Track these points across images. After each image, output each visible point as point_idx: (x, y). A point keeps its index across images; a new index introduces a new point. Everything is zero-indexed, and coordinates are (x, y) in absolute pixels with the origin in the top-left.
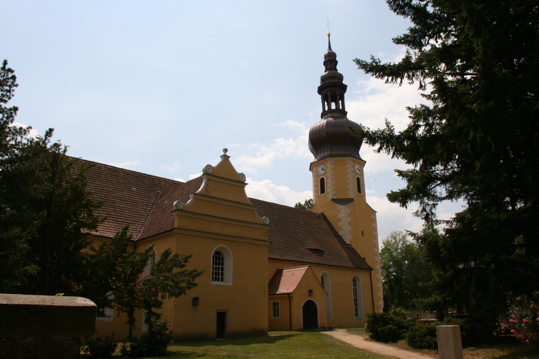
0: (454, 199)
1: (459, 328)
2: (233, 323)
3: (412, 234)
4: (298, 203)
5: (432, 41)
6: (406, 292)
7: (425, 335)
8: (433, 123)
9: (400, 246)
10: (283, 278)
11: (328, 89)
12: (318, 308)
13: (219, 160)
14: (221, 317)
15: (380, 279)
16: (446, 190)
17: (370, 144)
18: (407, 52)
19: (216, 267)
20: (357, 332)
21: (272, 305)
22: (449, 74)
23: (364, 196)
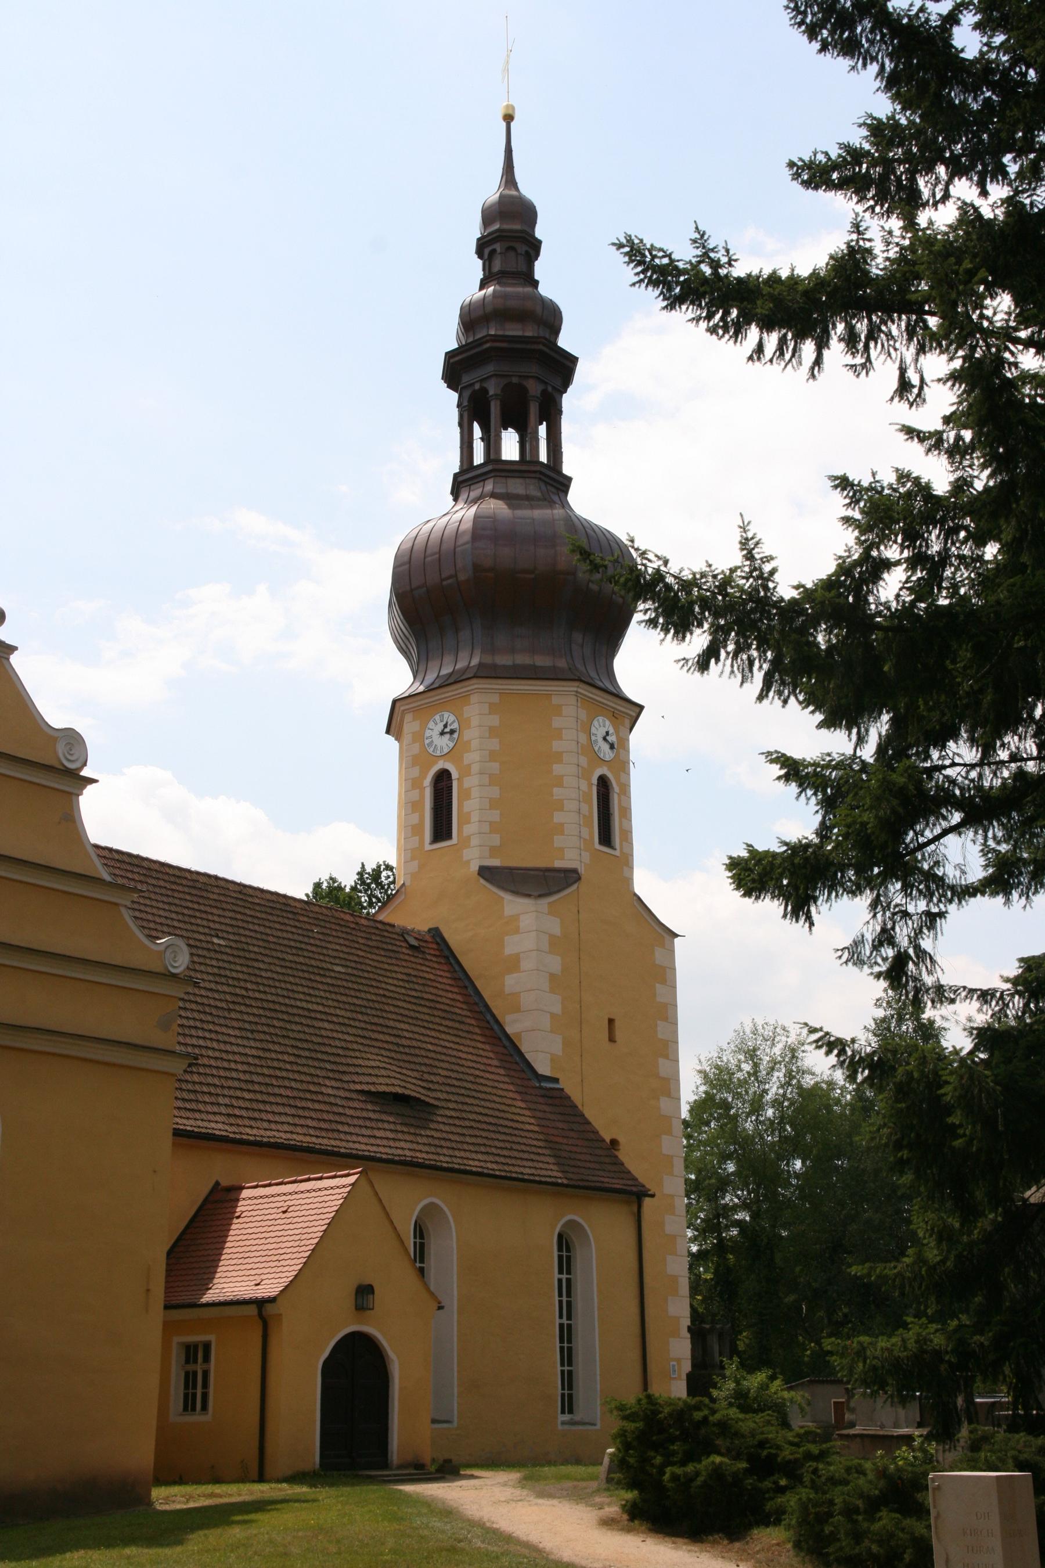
0: (1015, 895)
1: (1031, 1480)
3: (832, 1045)
4: (324, 877)
5: (964, 189)
6: (791, 1298)
7: (874, 1505)
8: (944, 558)
9: (773, 1090)
10: (236, 1228)
11: (490, 369)
12: (391, 1354)
15: (677, 1237)
16: (985, 851)
17: (666, 631)
18: (857, 228)
20: (569, 1484)
21: (176, 1357)
22: (1028, 343)
23: (627, 861)
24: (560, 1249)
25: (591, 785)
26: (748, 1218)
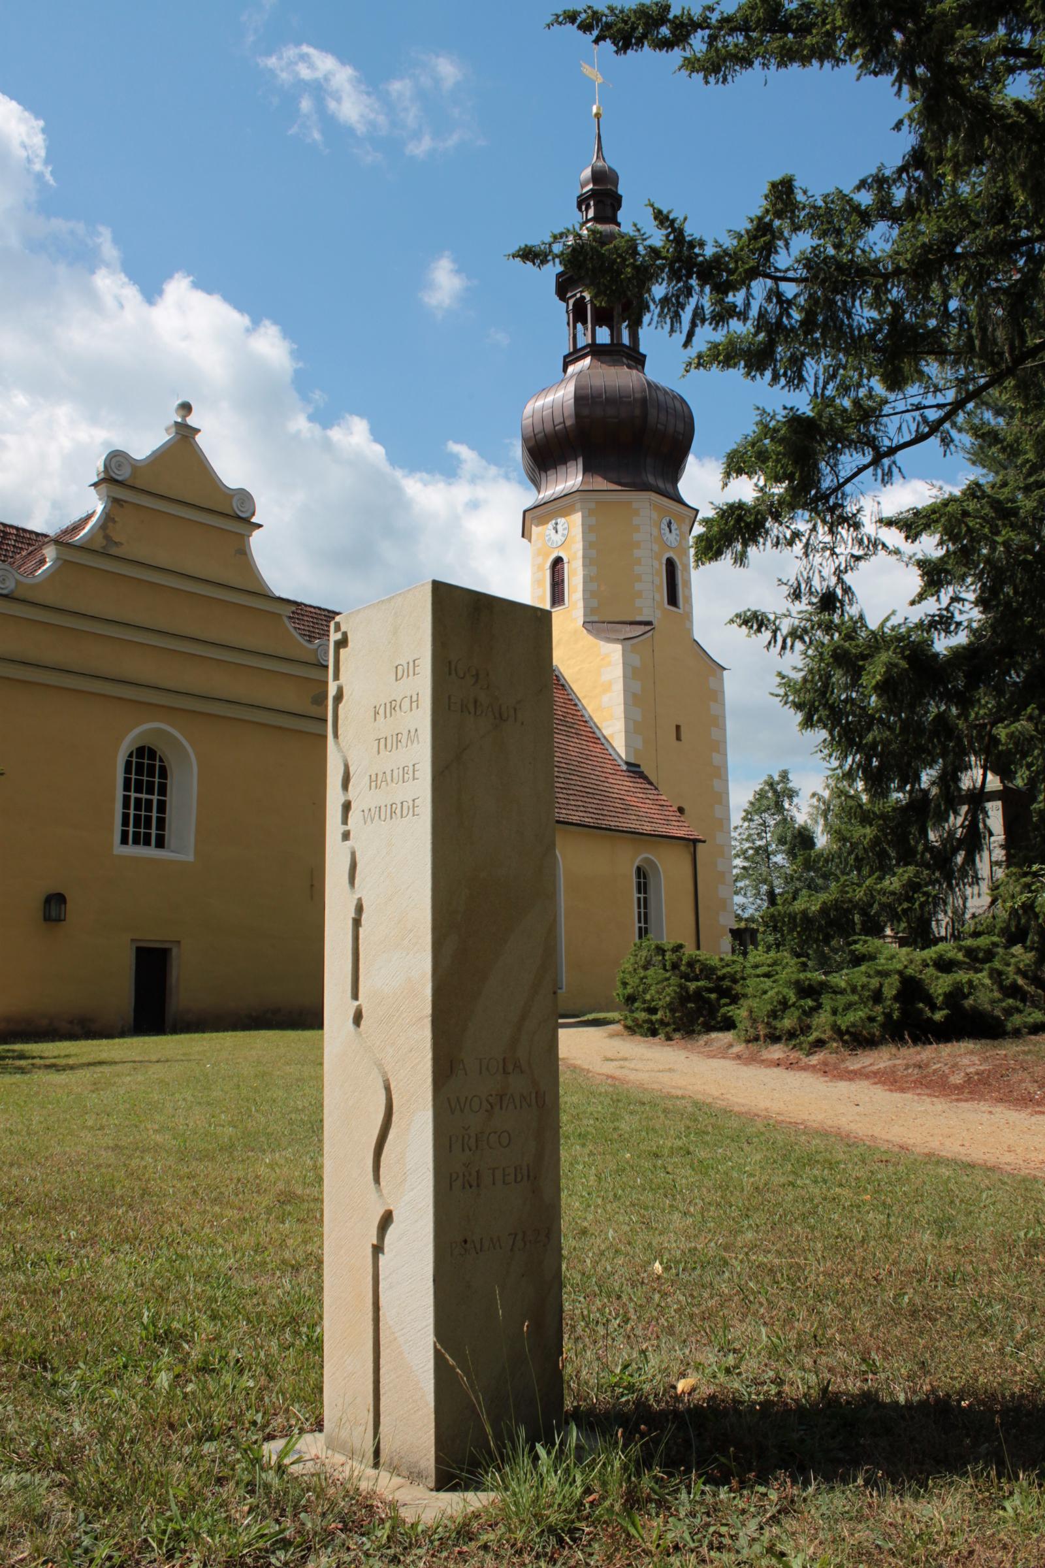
2: (187, 984)
14: (152, 964)
19: (138, 801)
23: (688, 616)
24: (639, 877)
25: (661, 563)
26: (626, 324)
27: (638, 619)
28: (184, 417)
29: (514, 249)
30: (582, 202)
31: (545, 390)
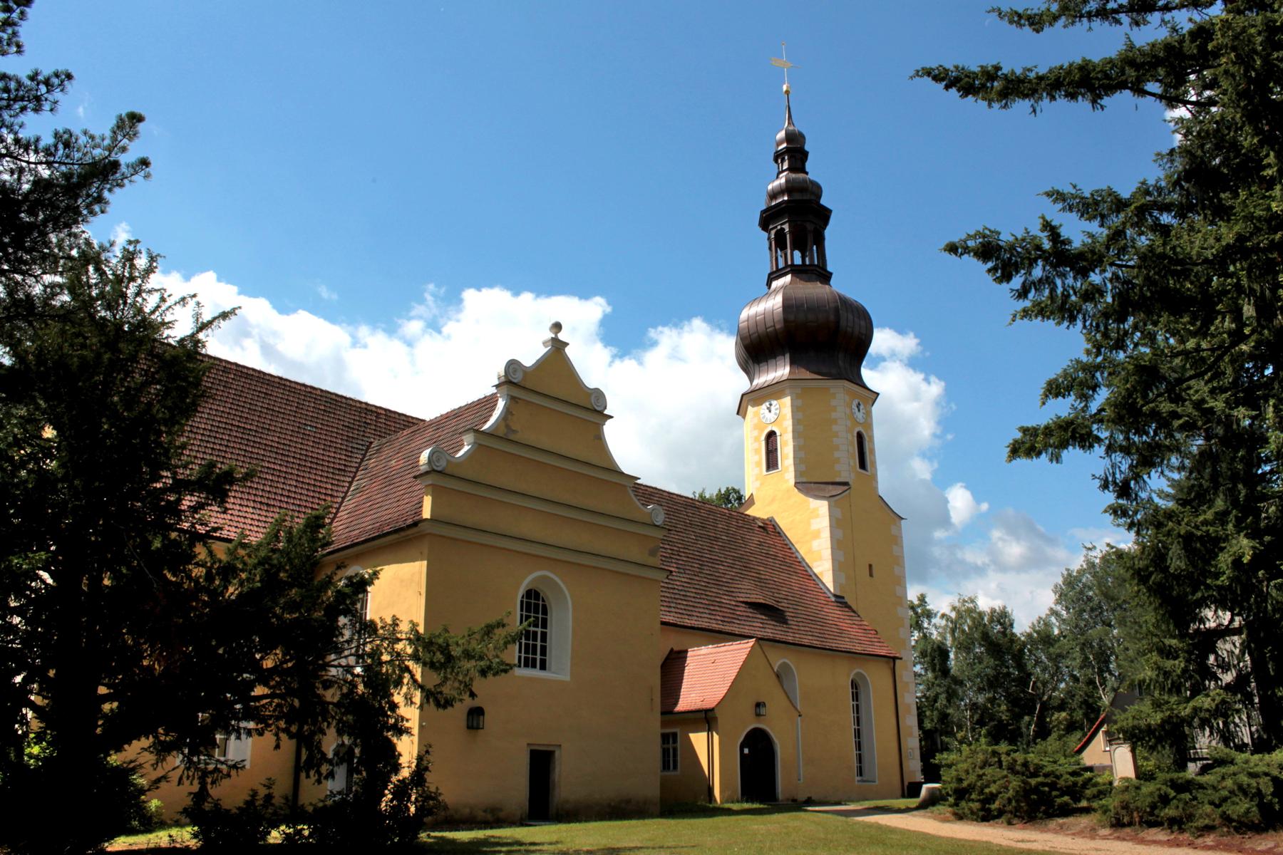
2: (569, 781)
12: (776, 740)
13: (542, 351)
14: (541, 762)
23: (874, 477)
27: (838, 480)
28: (556, 334)
29: (943, 246)
30: (778, 157)
31: (757, 300)
